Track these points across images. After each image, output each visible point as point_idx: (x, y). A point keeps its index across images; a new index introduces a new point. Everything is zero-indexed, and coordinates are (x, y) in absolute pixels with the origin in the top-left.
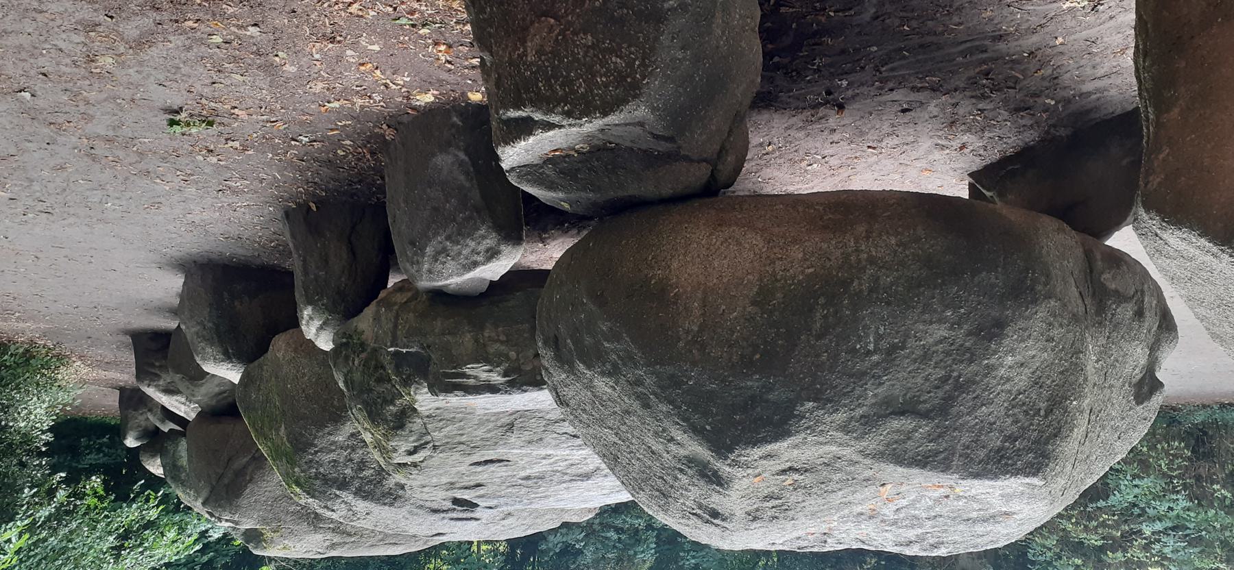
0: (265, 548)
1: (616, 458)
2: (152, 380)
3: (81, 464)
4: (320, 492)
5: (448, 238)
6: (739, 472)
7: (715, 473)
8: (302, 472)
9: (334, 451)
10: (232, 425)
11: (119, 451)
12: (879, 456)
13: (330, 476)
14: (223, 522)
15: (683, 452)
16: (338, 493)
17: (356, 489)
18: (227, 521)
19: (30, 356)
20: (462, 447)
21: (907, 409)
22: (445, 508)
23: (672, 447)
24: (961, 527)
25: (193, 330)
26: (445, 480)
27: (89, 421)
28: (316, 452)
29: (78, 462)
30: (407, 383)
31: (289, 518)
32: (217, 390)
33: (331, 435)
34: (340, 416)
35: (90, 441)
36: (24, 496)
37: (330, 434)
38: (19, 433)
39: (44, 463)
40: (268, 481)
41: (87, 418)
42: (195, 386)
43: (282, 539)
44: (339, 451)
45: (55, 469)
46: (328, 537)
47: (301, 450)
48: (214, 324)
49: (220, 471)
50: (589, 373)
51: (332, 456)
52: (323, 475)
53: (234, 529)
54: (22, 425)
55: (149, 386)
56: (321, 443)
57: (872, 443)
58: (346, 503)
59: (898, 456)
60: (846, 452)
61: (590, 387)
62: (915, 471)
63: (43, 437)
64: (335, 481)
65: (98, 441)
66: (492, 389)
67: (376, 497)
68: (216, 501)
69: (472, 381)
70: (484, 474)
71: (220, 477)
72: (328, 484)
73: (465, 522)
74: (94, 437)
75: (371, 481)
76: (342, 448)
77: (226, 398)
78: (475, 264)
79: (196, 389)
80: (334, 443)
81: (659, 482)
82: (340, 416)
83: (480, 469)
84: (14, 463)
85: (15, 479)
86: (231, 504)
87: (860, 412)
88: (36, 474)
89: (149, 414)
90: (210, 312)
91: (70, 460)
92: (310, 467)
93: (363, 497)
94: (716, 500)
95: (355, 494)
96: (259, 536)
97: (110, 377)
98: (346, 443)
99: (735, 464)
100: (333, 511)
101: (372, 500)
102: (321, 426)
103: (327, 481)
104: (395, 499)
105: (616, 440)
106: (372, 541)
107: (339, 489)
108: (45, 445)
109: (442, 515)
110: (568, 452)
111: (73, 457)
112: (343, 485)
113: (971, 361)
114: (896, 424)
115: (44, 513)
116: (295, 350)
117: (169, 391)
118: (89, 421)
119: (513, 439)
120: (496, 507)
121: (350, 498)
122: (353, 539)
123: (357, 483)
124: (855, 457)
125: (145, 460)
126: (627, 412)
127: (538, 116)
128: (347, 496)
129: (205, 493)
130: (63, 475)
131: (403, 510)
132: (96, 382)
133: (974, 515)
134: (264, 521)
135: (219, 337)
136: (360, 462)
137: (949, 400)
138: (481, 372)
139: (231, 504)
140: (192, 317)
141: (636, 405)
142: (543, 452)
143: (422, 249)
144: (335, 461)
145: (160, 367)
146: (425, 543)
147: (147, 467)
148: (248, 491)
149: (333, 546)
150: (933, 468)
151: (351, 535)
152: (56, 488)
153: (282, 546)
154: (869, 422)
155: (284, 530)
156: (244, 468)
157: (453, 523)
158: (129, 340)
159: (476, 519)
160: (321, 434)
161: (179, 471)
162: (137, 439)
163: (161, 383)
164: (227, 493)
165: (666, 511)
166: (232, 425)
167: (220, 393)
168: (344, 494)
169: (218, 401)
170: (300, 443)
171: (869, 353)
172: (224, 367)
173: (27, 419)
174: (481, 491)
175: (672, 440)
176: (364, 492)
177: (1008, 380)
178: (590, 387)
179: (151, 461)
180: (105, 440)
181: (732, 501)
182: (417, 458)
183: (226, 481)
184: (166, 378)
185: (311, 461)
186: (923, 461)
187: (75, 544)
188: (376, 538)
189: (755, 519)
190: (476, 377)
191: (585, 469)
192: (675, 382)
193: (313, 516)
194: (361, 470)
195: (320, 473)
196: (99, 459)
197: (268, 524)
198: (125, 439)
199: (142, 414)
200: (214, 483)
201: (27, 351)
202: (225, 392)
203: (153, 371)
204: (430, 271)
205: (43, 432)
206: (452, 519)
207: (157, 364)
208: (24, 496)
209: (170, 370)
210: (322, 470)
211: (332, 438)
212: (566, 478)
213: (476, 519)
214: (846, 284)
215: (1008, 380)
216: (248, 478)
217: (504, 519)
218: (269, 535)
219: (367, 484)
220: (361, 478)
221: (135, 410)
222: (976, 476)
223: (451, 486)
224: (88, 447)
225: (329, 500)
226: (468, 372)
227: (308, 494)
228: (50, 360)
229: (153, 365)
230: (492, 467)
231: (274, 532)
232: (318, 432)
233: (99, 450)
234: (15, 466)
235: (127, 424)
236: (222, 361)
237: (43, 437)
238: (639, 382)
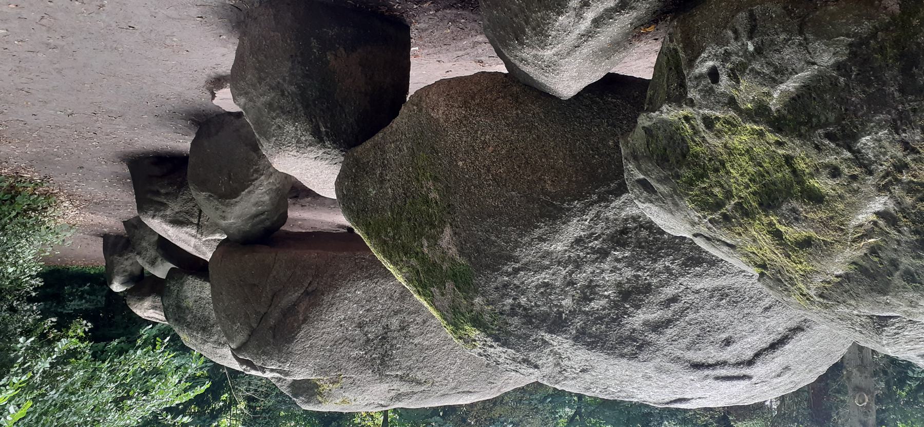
0: (320, 402)
2: (157, 210)
3: (65, 309)
4: (519, 337)
8: (489, 303)
9: (548, 267)
10: (273, 254)
11: (99, 297)
13: (536, 310)
14: (268, 372)
16: (547, 337)
17: (578, 330)
18: (272, 370)
19: (16, 192)
22: (711, 361)
25: (263, 99)
27: (70, 270)
28: (516, 271)
29: (63, 307)
31: (351, 365)
32: (254, 210)
33: (544, 240)
34: (561, 210)
35: (73, 288)
36: (19, 346)
37: (541, 239)
38: (8, 278)
39: (35, 308)
40: (326, 321)
41: (69, 269)
42: (227, 206)
43: (342, 391)
45: (45, 314)
46: (395, 387)
47: (488, 267)
48: (299, 87)
49: (263, 311)
51: (544, 277)
52: (525, 309)
53: (279, 379)
54: (10, 270)
55: (154, 217)
56: (526, 255)
58: (555, 354)
63: (33, 282)
64: (544, 317)
65: (80, 289)
67: (608, 344)
68: (259, 347)
71: (263, 317)
72: (531, 323)
73: (735, 382)
74: (76, 286)
75: (601, 318)
76: (559, 263)
77: (262, 221)
80: (547, 254)
82: (561, 210)
84: (4, 308)
85: (6, 325)
86: (280, 351)
88: (27, 319)
89: (138, 257)
90: (292, 68)
91: (55, 306)
92: (503, 296)
93: (588, 344)
95: (576, 339)
96: (312, 389)
97: (95, 222)
98: (567, 254)
100: (536, 367)
101: (602, 349)
102: (529, 226)
103: (531, 319)
104: (640, 348)
106: (444, 390)
107: (551, 332)
108: (35, 290)
109: (706, 372)
111: (58, 304)
112: (557, 324)
115: (44, 364)
116: (465, 104)
117: (177, 222)
118: (70, 270)
121: (566, 346)
122: (423, 388)
123: (579, 322)
125: (132, 303)
128: (561, 343)
129: (240, 338)
130: (54, 320)
131: (651, 364)
132: (84, 228)
134: (322, 370)
135: (306, 107)
136: (588, 287)
139: (280, 351)
140: (260, 80)
144: (546, 285)
145: (167, 194)
146: (499, 390)
147: (135, 311)
148: (301, 334)
149: (399, 397)
151: (420, 384)
152: (48, 332)
153: (341, 400)
155: (344, 380)
156: (295, 305)
158: (125, 170)
160: (526, 239)
161: (184, 313)
162: (123, 284)
163: (168, 212)
164: (274, 337)
166: (273, 254)
167: (256, 216)
169: (253, 226)
170: (486, 256)
172: (313, 155)
173: (14, 264)
176: (590, 335)
179: (138, 305)
180: (86, 287)
183: (272, 322)
184: (174, 207)
185: (505, 286)
187: (79, 397)
188: (449, 387)
193: (378, 362)
194: (586, 299)
195: (519, 305)
196: (82, 305)
197: (326, 374)
198: (111, 283)
199: (127, 259)
200: (255, 325)
201: (12, 187)
202: (262, 214)
203: (159, 199)
205: (32, 277)
206: (717, 378)
207: (163, 191)
208: (19, 346)
209: (191, 187)
210: (523, 300)
211: (545, 246)
213: (750, 378)
216: (301, 318)
217: (779, 376)
218: (326, 387)
219: (594, 323)
220: (586, 313)
221: (120, 256)
224: (71, 294)
225: (533, 350)
227: (497, 339)
228: (37, 198)
229: (158, 193)
231: (333, 383)
232: (521, 235)
233: (81, 297)
234: (5, 311)
235: (113, 270)
236: (310, 145)
237: (33, 282)
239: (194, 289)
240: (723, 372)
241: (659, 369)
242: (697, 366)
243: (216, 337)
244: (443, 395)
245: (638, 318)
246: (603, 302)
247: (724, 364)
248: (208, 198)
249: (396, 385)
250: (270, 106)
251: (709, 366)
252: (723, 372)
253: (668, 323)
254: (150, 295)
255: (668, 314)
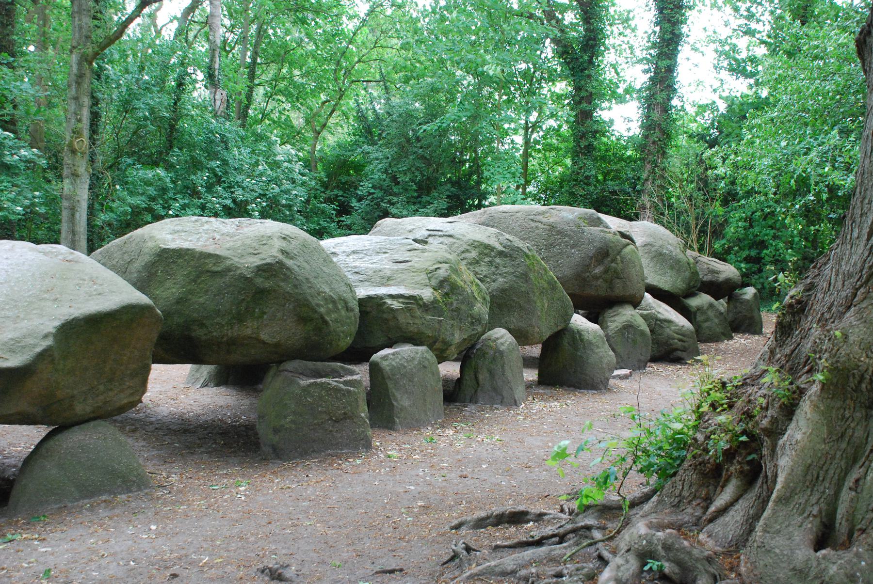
1: (325, 261)
5: (405, 367)
6: (275, 254)
7: (283, 254)
12: (225, 258)
15: (295, 262)
20: (414, 270)
21: (214, 274)
23: (299, 264)
24: (188, 229)
26: (426, 254)
30: (435, 301)
32: (616, 318)
42: (631, 322)
44: (502, 272)
46: (546, 219)
50: (331, 294)
51: (505, 270)
57: (228, 263)
59: (217, 258)
60: (236, 260)
61: (332, 289)
62: (212, 252)
64: (506, 256)
66: (392, 297)
69: (401, 300)
70: (406, 256)
78: (393, 354)
79: (629, 319)
80: (505, 277)
81: (306, 251)
83: (407, 259)
87: (231, 273)
94: (284, 244)
95: (494, 248)
99: (275, 257)
101: (485, 244)
105: (323, 268)
109: (447, 234)
110: (362, 265)
112: (501, 254)
113: (190, 290)
114: (219, 269)
119: (388, 273)
120: (404, 239)
124: (233, 258)
126: (315, 277)
127: (342, 385)
133: (183, 234)
137: (198, 277)
138: (395, 304)
140: (601, 358)
141: (312, 280)
142: (374, 266)
143: (419, 363)
149: (543, 213)
150: (206, 253)
154: (228, 269)
157: (441, 229)
159: (428, 230)
165: (304, 239)
168: (500, 248)
171: (227, 293)
174: (409, 247)
175: (299, 266)
177: (174, 284)
178: (332, 289)
179: (731, 275)
181: (278, 244)
182: (436, 266)
186: (210, 255)
189: (269, 237)
190: (399, 302)
191: (355, 256)
192: (295, 286)
194: (490, 262)
204: (417, 353)
211: (505, 280)
212: (365, 252)
213: (428, 230)
214: (233, 318)
215: (174, 284)
222: (188, 250)
223: (424, 251)
226: (402, 305)
229: (680, 340)
230: (401, 259)
238: (310, 287)
239: (666, 282)
240: (440, 233)
241: (464, 236)
242: (450, 236)
243: (653, 249)
244: (518, 212)
245: (474, 254)
246: (485, 260)
247: (440, 236)
248: (640, 326)
249: (544, 220)
250: (598, 347)
251: (446, 236)
252: (440, 233)
253: (463, 252)
254: (721, 282)
255: (463, 255)
